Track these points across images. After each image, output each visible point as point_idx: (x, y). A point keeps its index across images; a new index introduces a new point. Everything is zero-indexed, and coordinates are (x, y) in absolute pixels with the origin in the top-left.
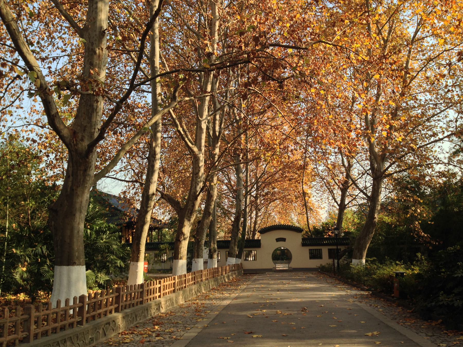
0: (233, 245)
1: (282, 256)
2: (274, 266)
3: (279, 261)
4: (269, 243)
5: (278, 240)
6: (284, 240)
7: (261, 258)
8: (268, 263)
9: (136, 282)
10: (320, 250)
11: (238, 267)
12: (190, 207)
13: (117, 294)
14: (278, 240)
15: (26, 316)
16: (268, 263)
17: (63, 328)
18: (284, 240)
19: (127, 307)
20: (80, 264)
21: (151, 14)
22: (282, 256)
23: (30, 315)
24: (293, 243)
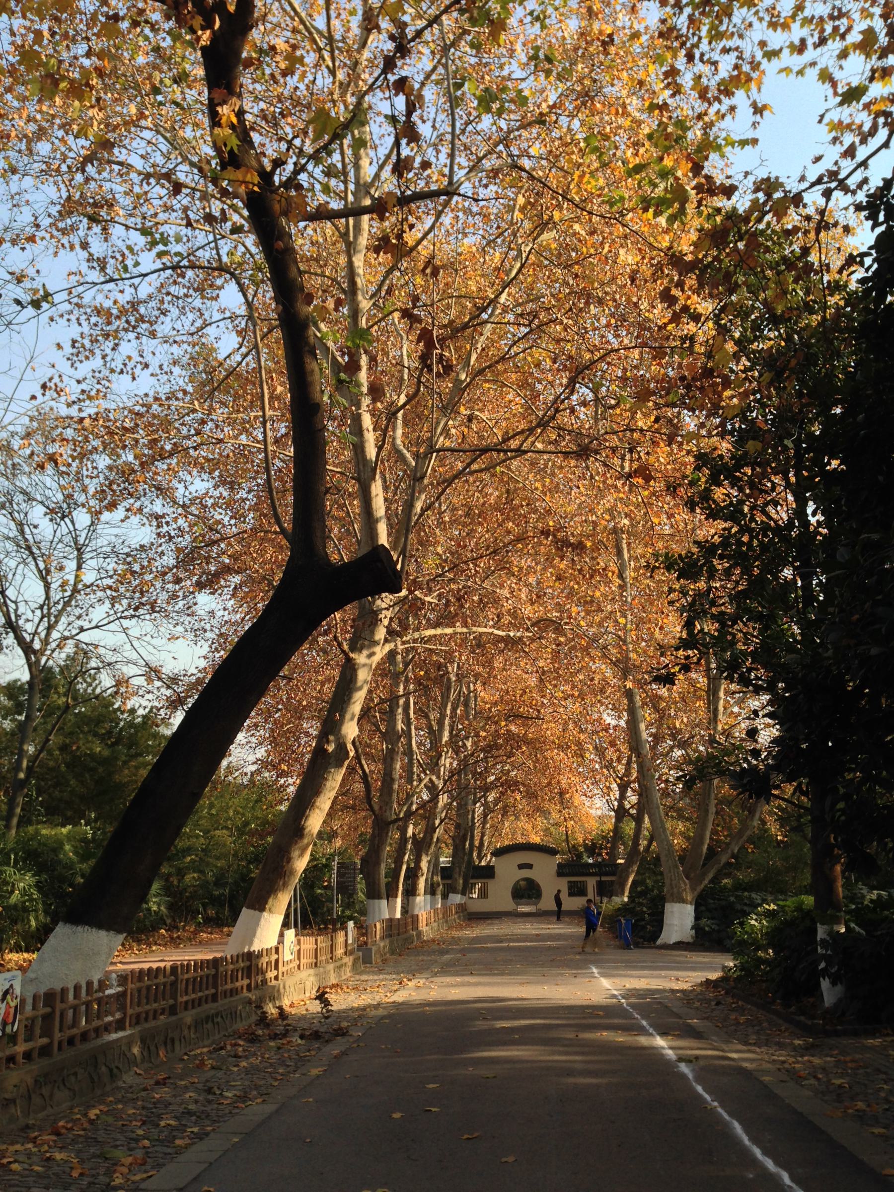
0: (456, 876)
1: (527, 891)
2: (515, 906)
3: (524, 900)
4: (508, 872)
5: (521, 867)
6: (529, 866)
7: (500, 895)
8: (508, 904)
9: (251, 943)
10: (584, 884)
11: (462, 908)
12: (428, 840)
13: (48, 1010)
14: (521, 867)
15: (48, 1010)
16: (508, 904)
17: (214, 998)
18: (529, 866)
19: (190, 1006)
20: (683, 901)
21: (343, 291)
22: (527, 891)
23: (53, 1008)
24: (544, 872)
